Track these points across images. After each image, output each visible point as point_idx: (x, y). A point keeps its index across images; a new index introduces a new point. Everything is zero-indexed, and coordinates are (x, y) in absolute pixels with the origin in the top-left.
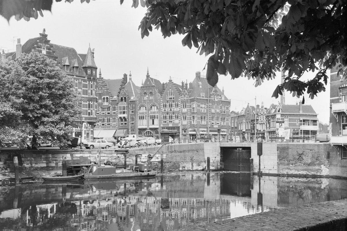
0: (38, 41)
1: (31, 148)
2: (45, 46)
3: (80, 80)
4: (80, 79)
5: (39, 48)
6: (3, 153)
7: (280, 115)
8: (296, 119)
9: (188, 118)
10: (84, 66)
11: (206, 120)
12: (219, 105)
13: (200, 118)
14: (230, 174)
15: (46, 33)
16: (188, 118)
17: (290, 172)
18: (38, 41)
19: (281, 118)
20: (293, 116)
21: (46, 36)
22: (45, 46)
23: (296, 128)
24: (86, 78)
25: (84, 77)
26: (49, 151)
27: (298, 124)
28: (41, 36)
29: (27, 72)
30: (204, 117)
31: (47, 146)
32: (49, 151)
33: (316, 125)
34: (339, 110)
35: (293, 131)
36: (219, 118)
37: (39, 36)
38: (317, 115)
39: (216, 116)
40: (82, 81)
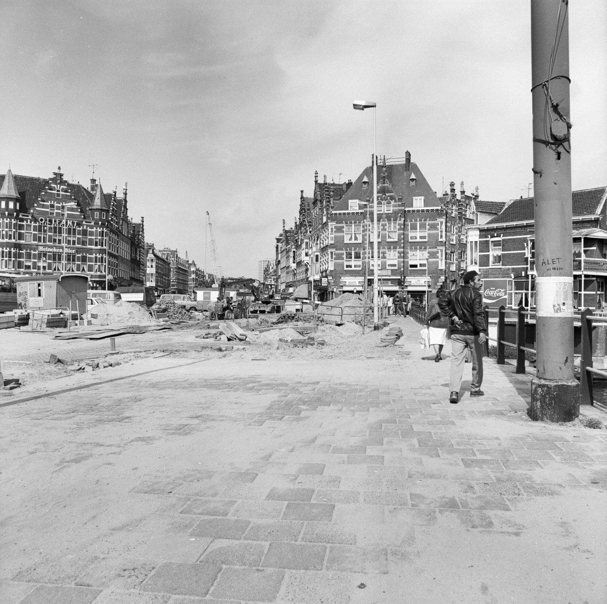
0: (50, 182)
2: (60, 187)
3: (85, 226)
5: (52, 190)
6: (525, 395)
7: (478, 233)
10: (411, 178)
12: (454, 226)
15: (61, 172)
17: (119, 381)
18: (50, 182)
19: (480, 241)
20: (518, 230)
21: (61, 175)
22: (60, 187)
24: (93, 224)
25: (90, 223)
28: (55, 176)
35: (515, 278)
37: (53, 176)
40: (88, 228)
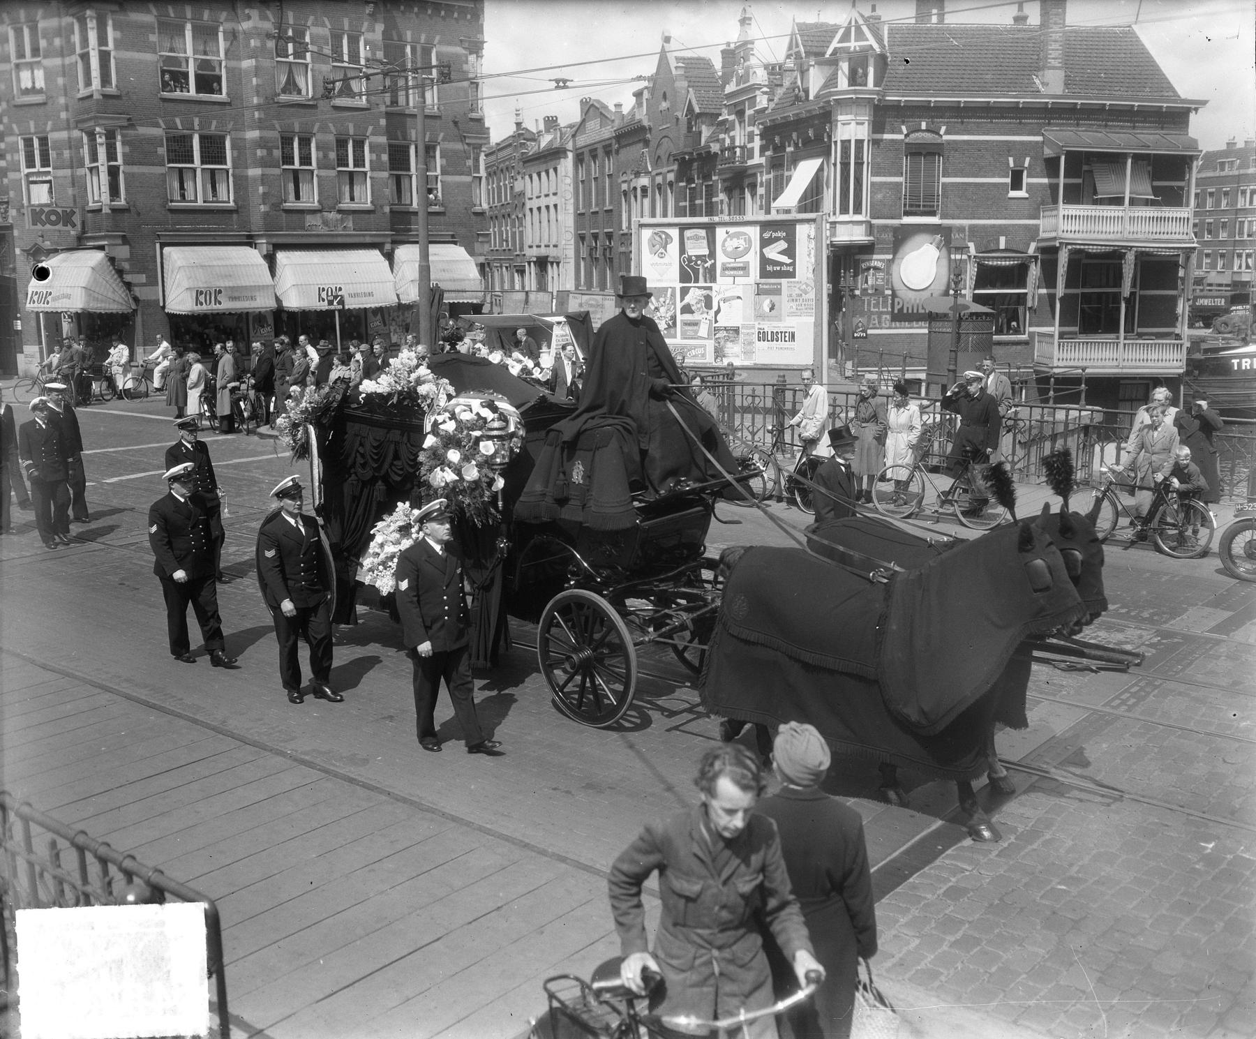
1: (843, 468)
4: (628, 710)
8: (1009, 148)
9: (59, 146)
11: (229, 165)
13: (162, 151)
14: (690, 427)
16: (60, 155)
23: (1002, 230)
26: (1122, 382)
27: (1022, 194)
29: (668, 624)
30: (203, 139)
31: (146, 701)
32: (1122, 382)
33: (1172, 198)
34: (162, 272)
36: (359, 145)
38: (1192, 116)
39: (324, 129)
